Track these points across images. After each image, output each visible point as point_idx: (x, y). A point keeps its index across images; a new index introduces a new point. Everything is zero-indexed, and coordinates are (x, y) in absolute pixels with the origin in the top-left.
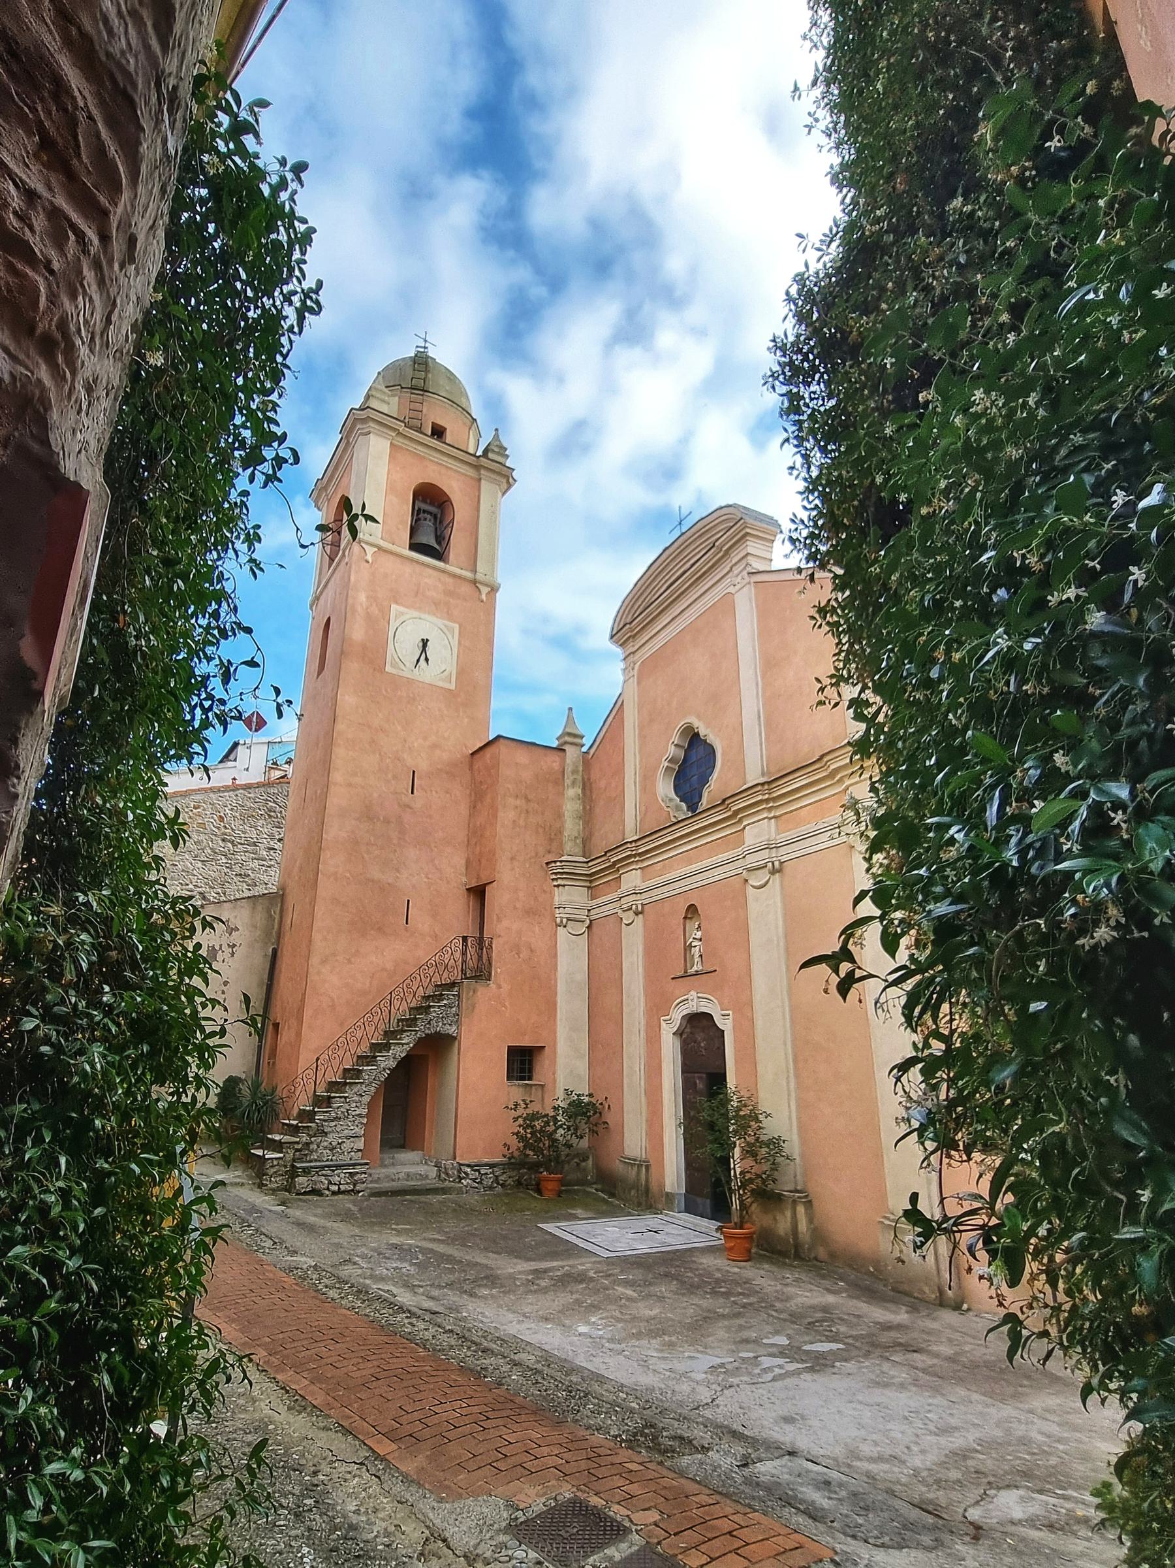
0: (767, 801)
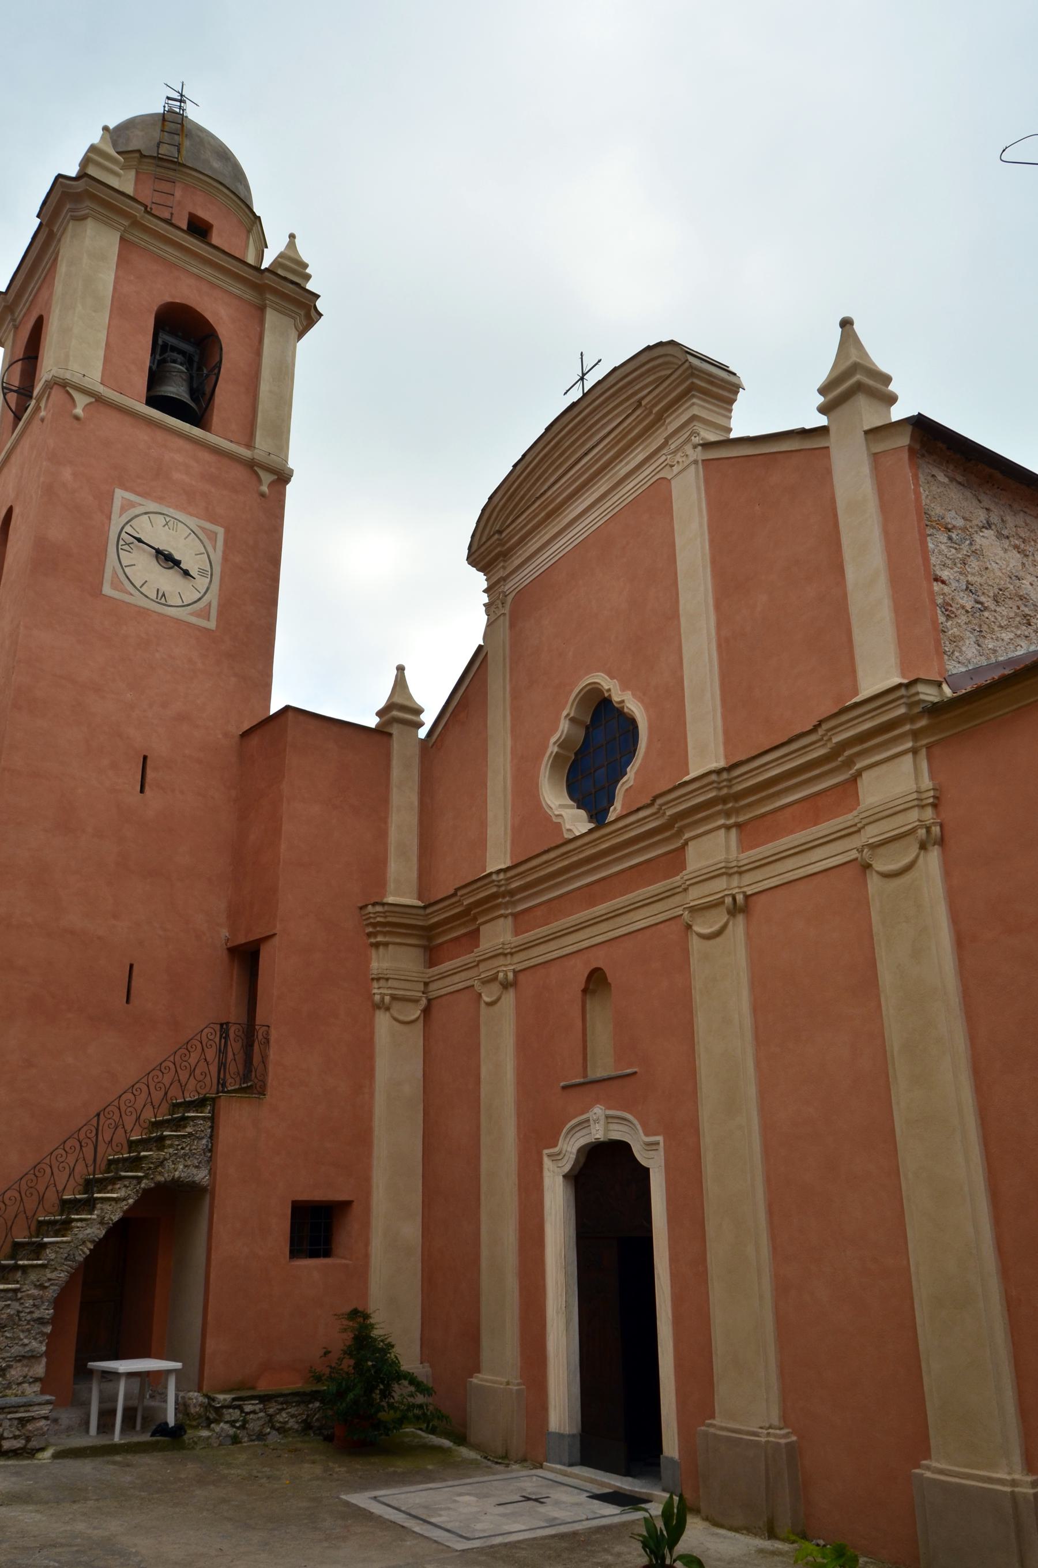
0: (724, 800)
